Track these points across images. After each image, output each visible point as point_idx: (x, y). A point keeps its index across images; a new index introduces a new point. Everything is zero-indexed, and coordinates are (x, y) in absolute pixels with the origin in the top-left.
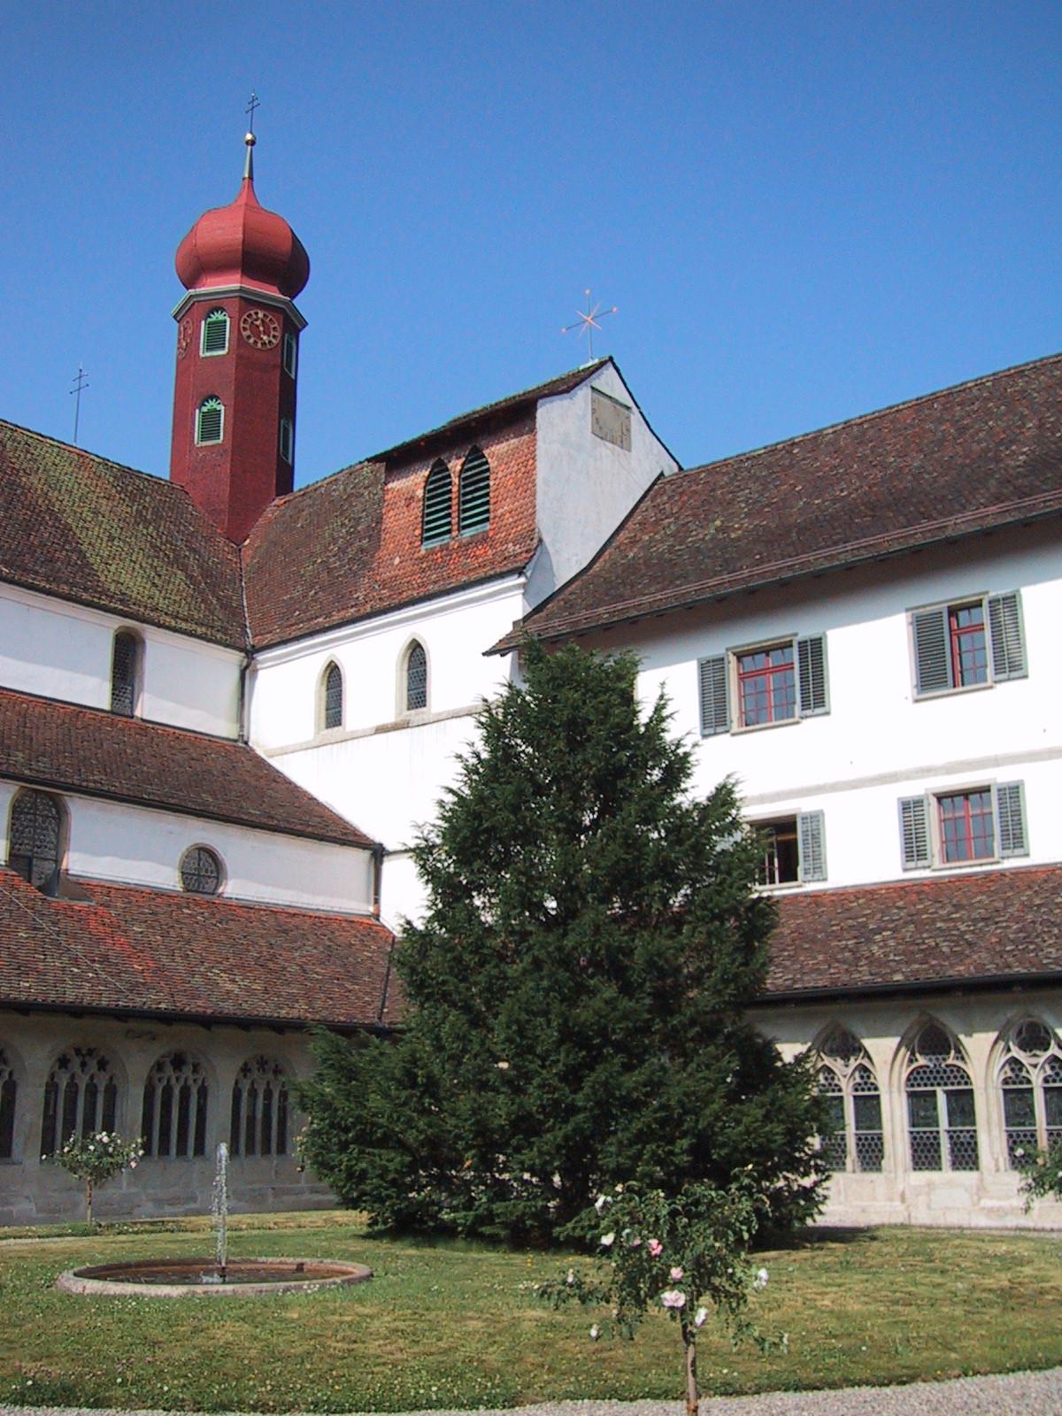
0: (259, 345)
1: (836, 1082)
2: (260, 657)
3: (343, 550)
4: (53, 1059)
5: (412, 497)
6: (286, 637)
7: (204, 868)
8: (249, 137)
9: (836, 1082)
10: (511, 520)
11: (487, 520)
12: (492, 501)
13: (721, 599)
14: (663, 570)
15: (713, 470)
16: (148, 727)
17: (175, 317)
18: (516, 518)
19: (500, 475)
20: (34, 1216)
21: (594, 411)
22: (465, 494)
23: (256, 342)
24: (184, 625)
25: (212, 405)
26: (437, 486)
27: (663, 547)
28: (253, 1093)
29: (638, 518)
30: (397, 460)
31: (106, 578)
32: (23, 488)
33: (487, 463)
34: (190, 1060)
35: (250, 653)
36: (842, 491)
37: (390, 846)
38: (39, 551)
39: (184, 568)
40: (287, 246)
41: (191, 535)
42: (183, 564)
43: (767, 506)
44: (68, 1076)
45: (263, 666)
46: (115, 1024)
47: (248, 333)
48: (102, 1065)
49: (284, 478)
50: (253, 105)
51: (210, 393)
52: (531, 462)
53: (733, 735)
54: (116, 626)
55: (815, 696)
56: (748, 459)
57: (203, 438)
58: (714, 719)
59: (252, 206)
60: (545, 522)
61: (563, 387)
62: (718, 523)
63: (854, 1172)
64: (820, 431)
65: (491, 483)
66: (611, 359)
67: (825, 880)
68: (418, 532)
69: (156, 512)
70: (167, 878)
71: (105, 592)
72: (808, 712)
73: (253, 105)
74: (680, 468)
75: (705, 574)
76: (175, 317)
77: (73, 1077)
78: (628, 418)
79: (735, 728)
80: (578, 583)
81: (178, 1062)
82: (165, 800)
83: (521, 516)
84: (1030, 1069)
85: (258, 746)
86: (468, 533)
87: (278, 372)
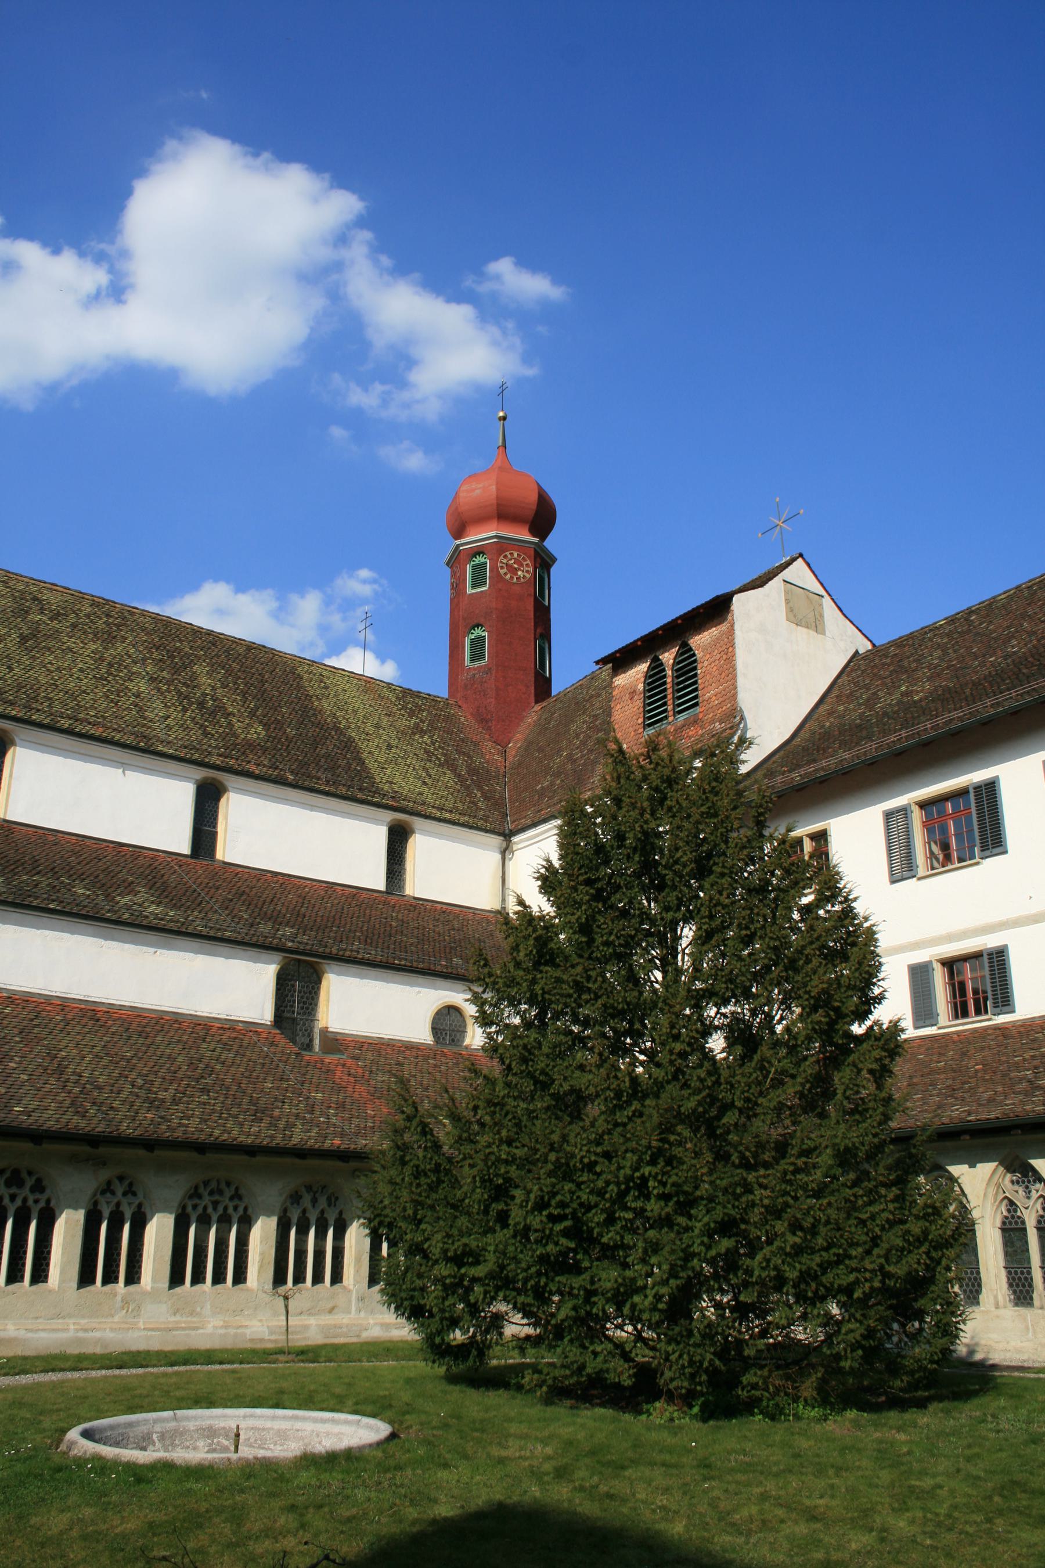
0: (515, 580)
1: (1019, 1214)
2: (515, 839)
3: (584, 743)
4: (284, 1196)
5: (635, 691)
8: (501, 414)
9: (1019, 1214)
11: (696, 704)
12: (700, 687)
13: (899, 754)
14: (853, 733)
15: (899, 643)
16: (420, 905)
17: (448, 564)
21: (787, 601)
22: (679, 684)
23: (511, 578)
24: (448, 816)
25: (478, 632)
26: (655, 678)
27: (855, 715)
29: (835, 692)
30: (620, 660)
31: (381, 778)
32: (315, 710)
33: (694, 655)
36: (1013, 647)
38: (323, 760)
39: (454, 769)
40: (534, 497)
41: (463, 740)
42: (452, 765)
43: (948, 668)
44: (299, 1211)
45: (520, 846)
46: (340, 1164)
47: (505, 570)
49: (543, 686)
51: (476, 622)
52: (731, 649)
53: (919, 879)
54: (389, 820)
55: (992, 840)
56: (931, 630)
57: (472, 660)
58: (902, 867)
59: (505, 468)
60: (746, 699)
62: (903, 688)
63: (1005, 1307)
64: (994, 598)
65: (699, 672)
67: (1013, 1011)
68: (640, 720)
69: (431, 724)
70: (421, 1034)
71: (377, 792)
72: (987, 853)
74: (874, 645)
75: (885, 733)
76: (448, 564)
77: (304, 1211)
78: (821, 605)
79: (922, 871)
80: (782, 753)
82: (415, 964)
84: (1023, 1210)
86: (682, 717)
87: (532, 599)
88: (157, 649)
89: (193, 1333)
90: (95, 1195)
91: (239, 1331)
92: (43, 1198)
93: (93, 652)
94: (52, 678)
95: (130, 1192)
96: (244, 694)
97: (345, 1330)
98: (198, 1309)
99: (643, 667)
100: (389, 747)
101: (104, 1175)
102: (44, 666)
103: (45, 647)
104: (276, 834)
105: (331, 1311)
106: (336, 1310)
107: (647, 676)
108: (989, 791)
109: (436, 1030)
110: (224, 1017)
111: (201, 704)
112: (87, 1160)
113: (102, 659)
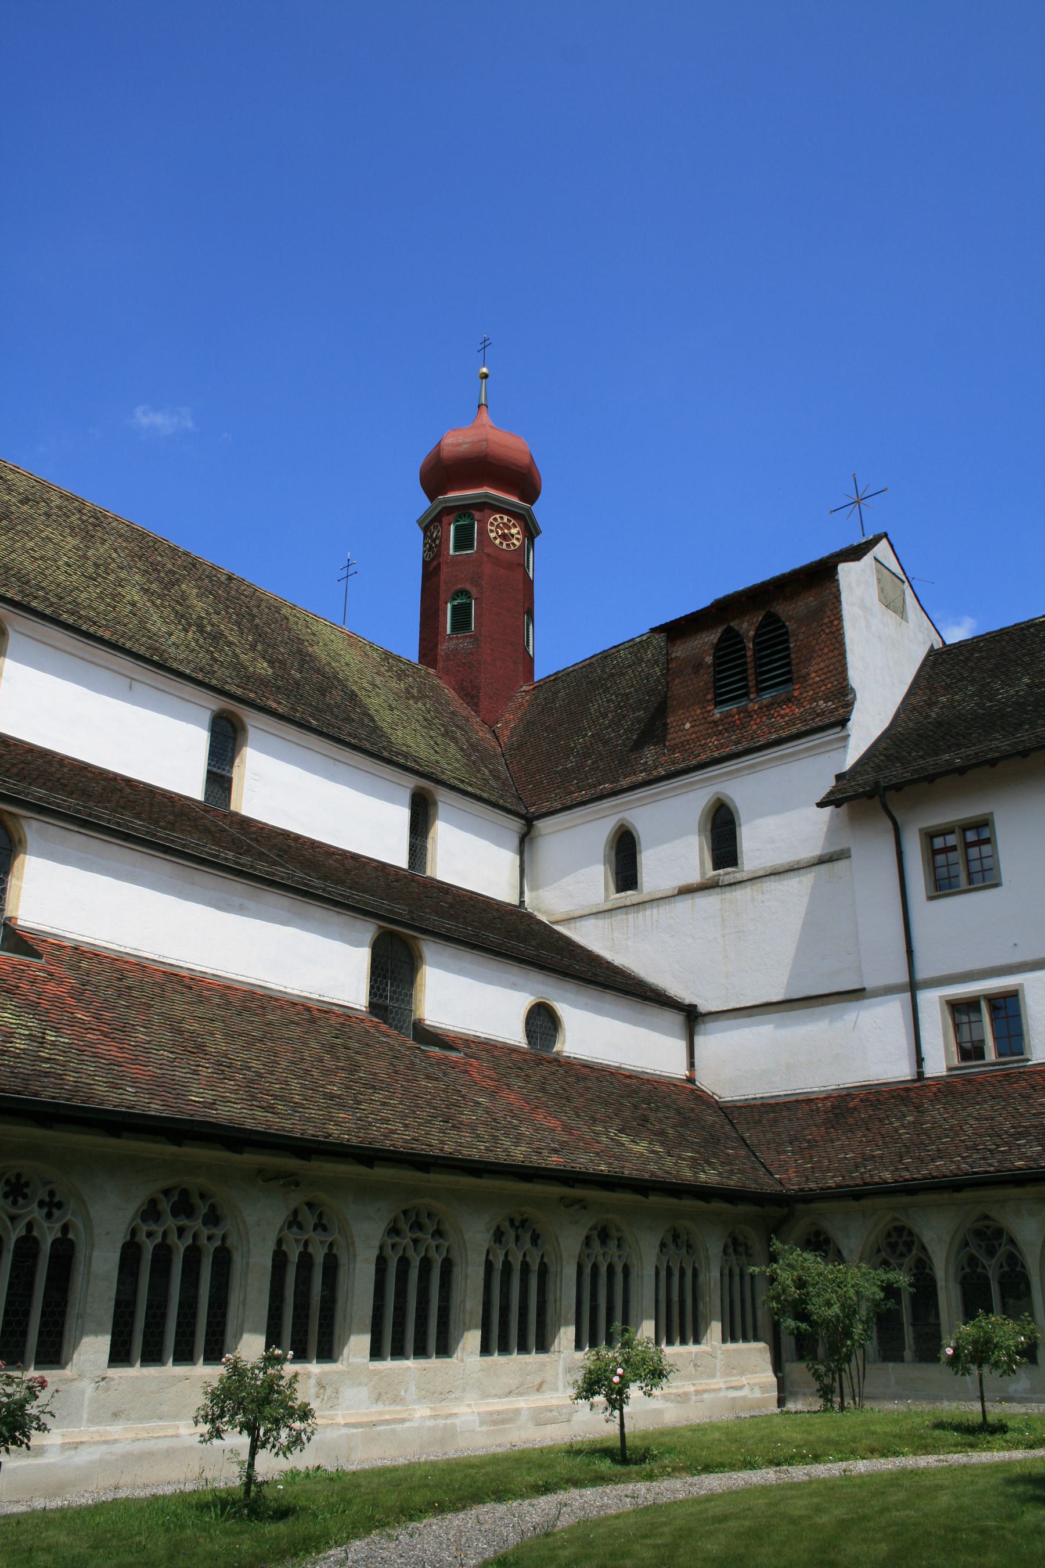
2: (541, 825)
6: (569, 803)
7: (542, 1021)
8: (484, 370)
10: (818, 679)
12: (794, 662)
18: (823, 677)
19: (801, 637)
20: (478, 1429)
28: (669, 1270)
34: (613, 1233)
35: (529, 822)
37: (704, 1007)
48: (535, 1239)
50: (485, 344)
52: (836, 623)
61: (855, 553)
65: (792, 645)
66: (886, 535)
70: (515, 1035)
73: (485, 344)
74: (944, 642)
81: (604, 1235)
83: (829, 675)
85: (539, 911)
88: (140, 559)
89: (399, 1427)
90: (281, 1230)
91: (449, 1421)
92: (218, 1232)
93: (74, 547)
94: (39, 567)
95: (321, 1226)
96: (238, 624)
97: (555, 1413)
98: (402, 1393)
99: (712, 637)
100: (391, 708)
101: (296, 1199)
102: (27, 552)
103: (22, 531)
104: (287, 789)
105: (539, 1388)
106: (544, 1387)
107: (717, 648)
108: (984, 823)
109: (530, 1033)
110: (317, 997)
111: (201, 629)
112: (276, 1178)
113: (85, 557)
